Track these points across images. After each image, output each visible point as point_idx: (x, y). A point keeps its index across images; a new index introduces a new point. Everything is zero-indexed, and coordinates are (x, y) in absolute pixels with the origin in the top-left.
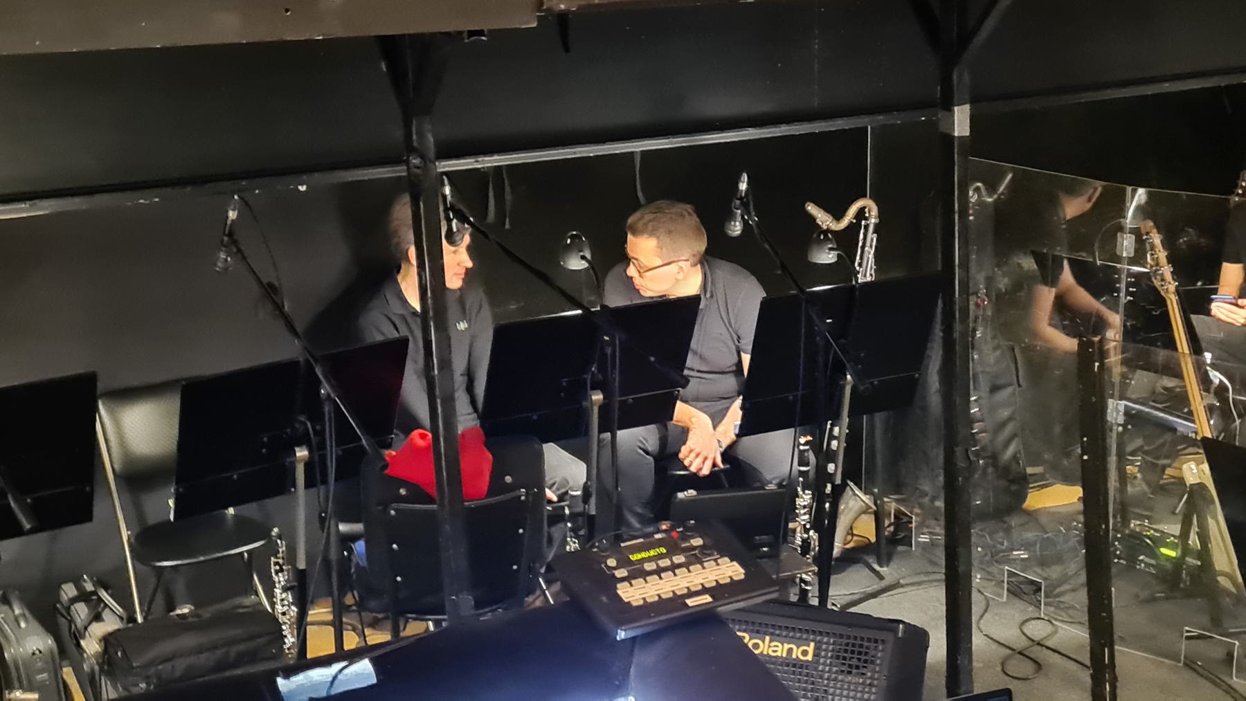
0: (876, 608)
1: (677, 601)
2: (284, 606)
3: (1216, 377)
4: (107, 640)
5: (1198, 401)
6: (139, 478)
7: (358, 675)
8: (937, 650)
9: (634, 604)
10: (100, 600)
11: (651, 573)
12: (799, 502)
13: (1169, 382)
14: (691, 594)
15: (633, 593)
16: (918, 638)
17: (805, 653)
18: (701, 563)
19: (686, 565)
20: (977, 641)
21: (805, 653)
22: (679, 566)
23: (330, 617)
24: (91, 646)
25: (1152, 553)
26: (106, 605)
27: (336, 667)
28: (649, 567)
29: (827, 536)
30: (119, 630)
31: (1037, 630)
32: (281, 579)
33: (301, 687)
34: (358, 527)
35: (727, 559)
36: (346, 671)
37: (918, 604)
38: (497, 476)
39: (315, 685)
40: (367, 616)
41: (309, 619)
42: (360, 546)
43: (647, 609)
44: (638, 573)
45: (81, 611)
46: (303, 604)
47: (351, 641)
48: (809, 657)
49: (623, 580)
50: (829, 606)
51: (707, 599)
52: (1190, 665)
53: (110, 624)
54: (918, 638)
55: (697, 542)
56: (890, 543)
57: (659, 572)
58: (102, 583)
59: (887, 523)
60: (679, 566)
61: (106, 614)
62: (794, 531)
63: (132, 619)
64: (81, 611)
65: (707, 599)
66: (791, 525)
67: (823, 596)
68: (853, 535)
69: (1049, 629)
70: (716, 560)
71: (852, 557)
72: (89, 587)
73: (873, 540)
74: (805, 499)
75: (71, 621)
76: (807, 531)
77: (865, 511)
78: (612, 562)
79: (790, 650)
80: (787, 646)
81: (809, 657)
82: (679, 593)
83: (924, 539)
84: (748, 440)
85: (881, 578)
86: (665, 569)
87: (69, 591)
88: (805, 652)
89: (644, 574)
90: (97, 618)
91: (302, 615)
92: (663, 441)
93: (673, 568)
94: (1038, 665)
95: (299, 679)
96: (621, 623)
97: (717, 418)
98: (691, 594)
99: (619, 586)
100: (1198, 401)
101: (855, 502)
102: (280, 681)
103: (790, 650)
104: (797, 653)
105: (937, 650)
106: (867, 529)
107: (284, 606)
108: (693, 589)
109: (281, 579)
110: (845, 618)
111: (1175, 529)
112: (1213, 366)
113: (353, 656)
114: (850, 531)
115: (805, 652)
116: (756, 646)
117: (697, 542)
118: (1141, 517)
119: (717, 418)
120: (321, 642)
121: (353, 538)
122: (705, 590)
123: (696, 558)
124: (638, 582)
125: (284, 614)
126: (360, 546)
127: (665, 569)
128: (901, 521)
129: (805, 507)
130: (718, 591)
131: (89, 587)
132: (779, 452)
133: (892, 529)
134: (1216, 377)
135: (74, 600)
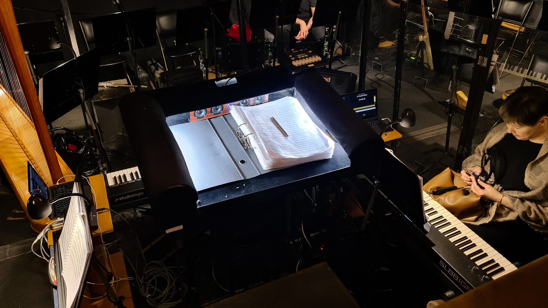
1: (306, 65)
2: (202, 67)
3: (430, 13)
5: (425, 20)
6: (165, 34)
7: (233, 82)
12: (325, 44)
13: (418, 15)
14: (309, 64)
15: (296, 63)
16: (355, 76)
19: (308, 57)
25: (409, 58)
27: (228, 79)
28: (299, 57)
29: (331, 53)
31: (380, 76)
32: (201, 61)
34: (220, 48)
37: (354, 70)
38: (253, 36)
39: (222, 84)
40: (222, 70)
42: (220, 53)
45: (153, 67)
51: (313, 65)
52: (415, 85)
53: (160, 71)
55: (310, 52)
56: (345, 55)
57: (302, 58)
58: (157, 61)
61: (159, 68)
63: (165, 70)
64: (153, 67)
65: (313, 65)
69: (382, 76)
72: (154, 62)
74: (326, 44)
75: (151, 70)
77: (339, 47)
78: (291, 56)
83: (354, 54)
84: (314, 28)
85: (343, 63)
87: (150, 62)
89: (298, 59)
92: (292, 29)
93: (305, 58)
94: (379, 85)
95: (219, 82)
96: (293, 71)
97: (307, 23)
98: (309, 64)
100: (425, 20)
101: (338, 44)
106: (340, 52)
109: (201, 61)
110: (336, 71)
111: (415, 52)
112: (430, 11)
113: (232, 77)
114: (336, 53)
117: (310, 52)
118: (407, 50)
119: (307, 23)
121: (219, 51)
122: (312, 63)
123: (310, 56)
126: (220, 53)
128: (348, 50)
130: (315, 63)
131: (154, 62)
132: (322, 31)
134: (430, 13)
135: (151, 65)
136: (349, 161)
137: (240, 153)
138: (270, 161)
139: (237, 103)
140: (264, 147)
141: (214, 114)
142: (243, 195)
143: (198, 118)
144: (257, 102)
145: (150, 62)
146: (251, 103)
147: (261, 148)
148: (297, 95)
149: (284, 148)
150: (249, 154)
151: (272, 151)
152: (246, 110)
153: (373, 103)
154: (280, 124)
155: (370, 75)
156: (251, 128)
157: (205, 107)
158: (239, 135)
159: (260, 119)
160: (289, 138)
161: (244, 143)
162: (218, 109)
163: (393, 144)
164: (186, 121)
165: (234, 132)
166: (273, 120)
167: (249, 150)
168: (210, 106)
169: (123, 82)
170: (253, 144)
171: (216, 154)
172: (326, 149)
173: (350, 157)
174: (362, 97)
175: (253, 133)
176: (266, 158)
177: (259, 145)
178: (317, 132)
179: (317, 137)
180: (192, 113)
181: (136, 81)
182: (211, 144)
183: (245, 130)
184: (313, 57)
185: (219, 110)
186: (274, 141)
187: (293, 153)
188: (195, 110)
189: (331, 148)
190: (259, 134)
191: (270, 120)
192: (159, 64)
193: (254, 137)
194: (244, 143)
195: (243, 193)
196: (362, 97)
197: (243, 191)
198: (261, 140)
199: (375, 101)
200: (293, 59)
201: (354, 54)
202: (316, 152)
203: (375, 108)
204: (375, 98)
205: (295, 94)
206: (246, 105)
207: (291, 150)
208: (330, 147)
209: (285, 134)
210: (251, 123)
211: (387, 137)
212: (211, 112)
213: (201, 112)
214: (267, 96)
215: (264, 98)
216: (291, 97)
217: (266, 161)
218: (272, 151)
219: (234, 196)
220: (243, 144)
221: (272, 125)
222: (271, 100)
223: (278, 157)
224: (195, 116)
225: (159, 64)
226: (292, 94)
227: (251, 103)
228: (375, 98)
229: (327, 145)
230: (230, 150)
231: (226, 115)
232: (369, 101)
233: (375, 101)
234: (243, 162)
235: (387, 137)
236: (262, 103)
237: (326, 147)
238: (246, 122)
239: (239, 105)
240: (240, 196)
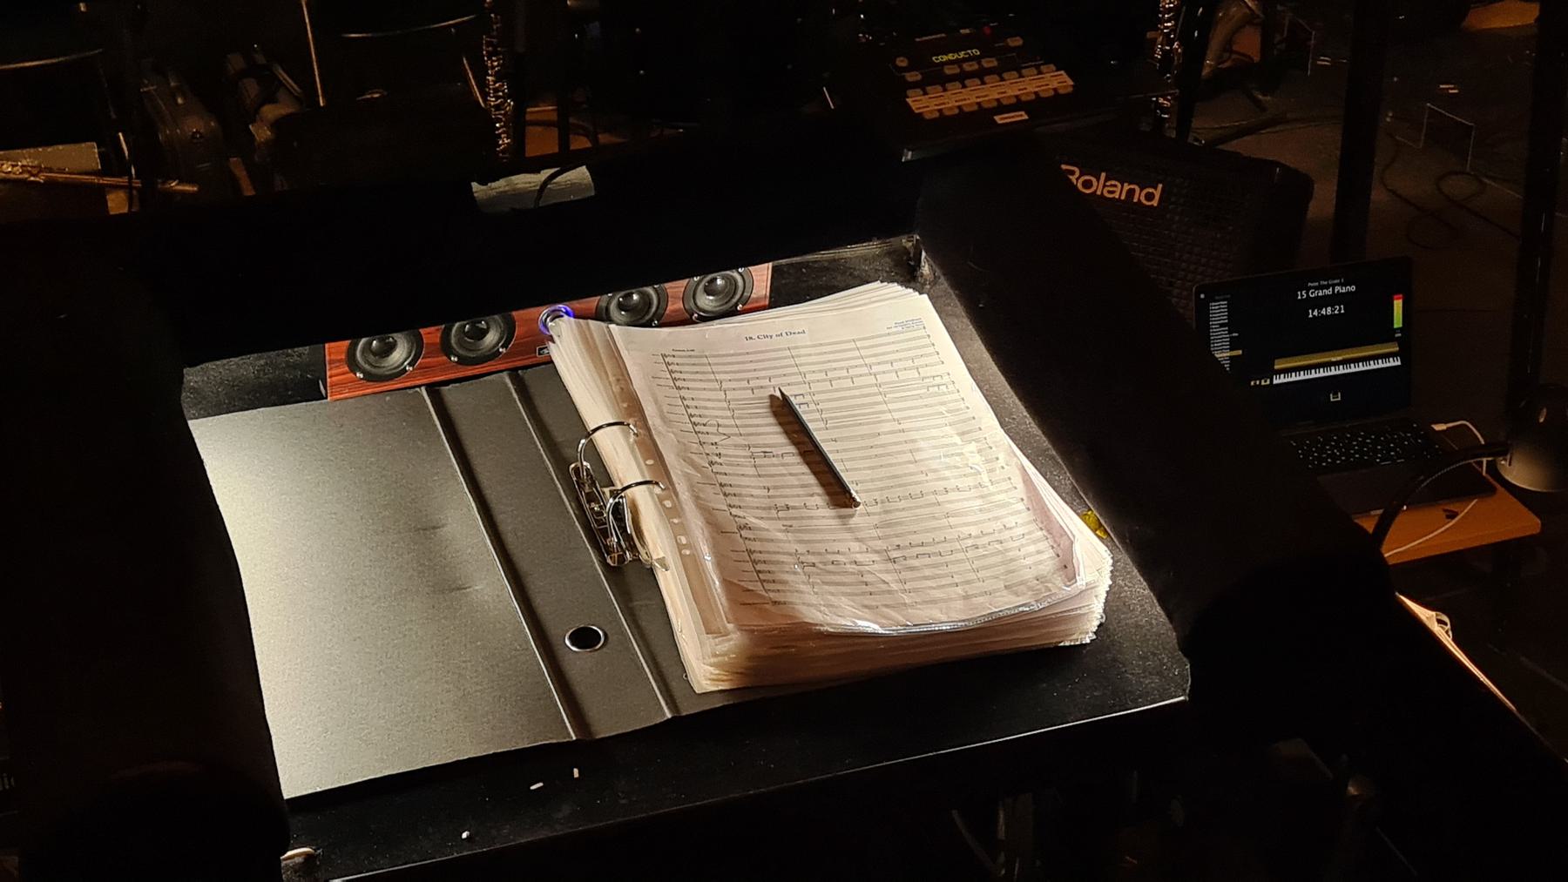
0: (1246, 146)
1: (983, 115)
2: (494, 96)
4: (276, 125)
7: (574, 187)
8: (1323, 202)
9: (928, 117)
10: (275, 77)
11: (952, 78)
14: (1002, 108)
15: (924, 103)
16: (1300, 186)
17: (1150, 197)
18: (1018, 70)
19: (999, 72)
20: (1378, 196)
21: (1150, 197)
22: (990, 71)
23: (554, 117)
24: (261, 133)
26: (281, 84)
29: (1195, 51)
30: (291, 115)
31: (1458, 186)
33: (502, 196)
35: (1052, 67)
36: (558, 179)
37: (1304, 147)
41: (528, 117)
43: (944, 122)
44: (936, 78)
45: (251, 88)
46: (523, 95)
47: (580, 143)
48: (1155, 203)
49: (915, 85)
50: (1190, 140)
54: (1300, 186)
55: (1016, 42)
57: (962, 78)
59: (1278, 38)
60: (990, 71)
61: (281, 94)
62: (1154, 41)
64: (251, 88)
66: (1150, 35)
67: (1184, 124)
68: (1232, 52)
70: (1038, 67)
71: (1236, 77)
72: (261, 59)
73: (1257, 59)
76: (1171, 43)
77: (1249, 20)
78: (902, 62)
79: (1131, 193)
80: (1127, 187)
81: (1155, 203)
82: (986, 106)
83: (1324, 61)
85: (1264, 110)
86: (971, 75)
87: (236, 62)
88: (1150, 196)
90: (271, 99)
91: (519, 111)
93: (981, 75)
99: (910, 92)
102: (475, 185)
103: (1131, 193)
104: (1140, 196)
105: (1323, 202)
106: (1250, 44)
107: (494, 96)
108: (1005, 102)
114: (1227, 47)
115: (1150, 196)
116: (1087, 184)
117: (1016, 42)
120: (541, 142)
122: (1018, 105)
123: (1011, 64)
124: (934, 90)
125: (498, 107)
127: (971, 75)
129: (1170, 10)
130: (1036, 106)
131: (261, 59)
133: (1283, 46)
136: (1182, 669)
137: (575, 587)
138: (732, 642)
139: (592, 302)
140: (708, 559)
141: (463, 361)
142: (560, 830)
143: (369, 377)
144: (707, 302)
145: (236, 62)
146: (675, 306)
147: (691, 566)
148: (934, 282)
149: (822, 567)
150: (625, 596)
151: (748, 585)
152: (639, 346)
153: (1386, 334)
154: (818, 436)
155: (1400, 183)
156: (649, 448)
157: (409, 323)
158: (586, 483)
159: (711, 404)
160: (858, 518)
161: (609, 535)
162: (484, 333)
163: (1431, 577)
164: (306, 389)
165: (561, 462)
166: (784, 412)
167: (632, 578)
168: (444, 317)
169: (76, 159)
170: (657, 543)
171: (444, 585)
172: (1060, 589)
173: (1189, 645)
174: (1326, 296)
175: (659, 475)
176: (710, 629)
177: (680, 547)
178: (1021, 491)
179: (1018, 519)
180: (335, 350)
181: (154, 160)
182: (424, 530)
183: (620, 456)
184: (1011, 76)
185: (491, 338)
186: (772, 528)
187: (861, 596)
188: (355, 337)
189: (1090, 588)
190: (692, 487)
191: (765, 410)
192: (283, 75)
193: (661, 500)
194: (605, 534)
195: (562, 822)
196: (1326, 296)
197: (566, 810)
198: (696, 522)
199: (1398, 322)
200: (913, 77)
201: (1324, 61)
202: (1004, 603)
203: (1395, 362)
204: (1398, 305)
205: (926, 269)
206: (642, 317)
207: (864, 589)
208: (1081, 582)
209: (839, 495)
210: (653, 420)
211: (1414, 538)
212: (446, 349)
213: (389, 349)
214: (761, 276)
215: (748, 283)
216: (896, 288)
217: (710, 641)
218: (748, 585)
219: (515, 835)
220: (597, 535)
221: (774, 436)
222: (783, 295)
223: (781, 623)
224: (353, 365)
225: (283, 75)
226: (907, 275)
227: (675, 306)
228: (1398, 305)
229: (1067, 567)
230: (523, 564)
231: (532, 372)
232: (1362, 325)
233: (1398, 322)
234: (584, 638)
235: (1414, 538)
236: (733, 312)
237: (1058, 581)
238: (631, 410)
239: (603, 316)
240: (543, 834)
